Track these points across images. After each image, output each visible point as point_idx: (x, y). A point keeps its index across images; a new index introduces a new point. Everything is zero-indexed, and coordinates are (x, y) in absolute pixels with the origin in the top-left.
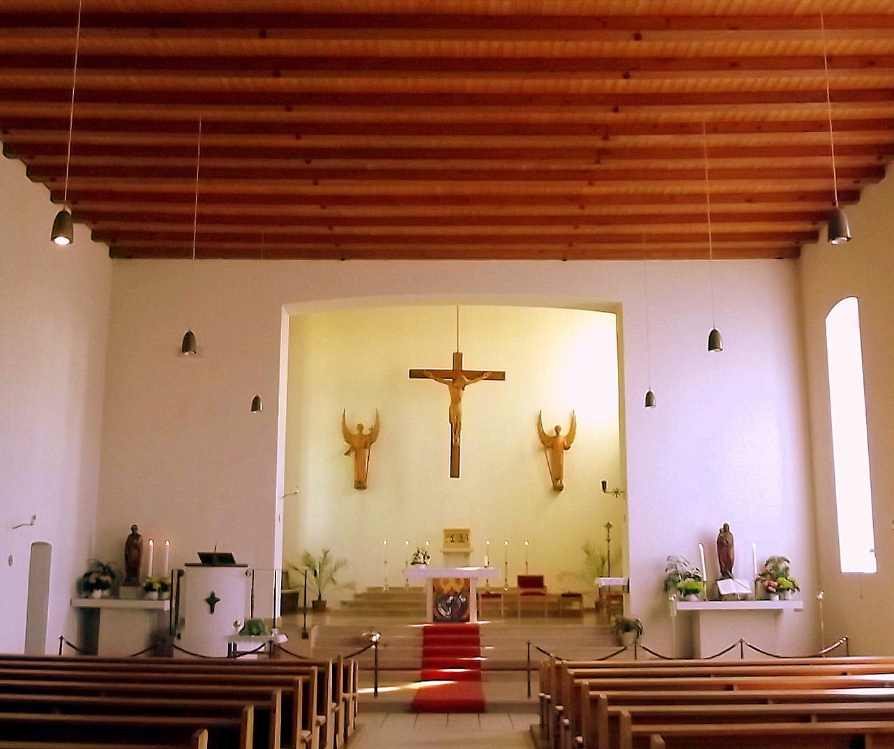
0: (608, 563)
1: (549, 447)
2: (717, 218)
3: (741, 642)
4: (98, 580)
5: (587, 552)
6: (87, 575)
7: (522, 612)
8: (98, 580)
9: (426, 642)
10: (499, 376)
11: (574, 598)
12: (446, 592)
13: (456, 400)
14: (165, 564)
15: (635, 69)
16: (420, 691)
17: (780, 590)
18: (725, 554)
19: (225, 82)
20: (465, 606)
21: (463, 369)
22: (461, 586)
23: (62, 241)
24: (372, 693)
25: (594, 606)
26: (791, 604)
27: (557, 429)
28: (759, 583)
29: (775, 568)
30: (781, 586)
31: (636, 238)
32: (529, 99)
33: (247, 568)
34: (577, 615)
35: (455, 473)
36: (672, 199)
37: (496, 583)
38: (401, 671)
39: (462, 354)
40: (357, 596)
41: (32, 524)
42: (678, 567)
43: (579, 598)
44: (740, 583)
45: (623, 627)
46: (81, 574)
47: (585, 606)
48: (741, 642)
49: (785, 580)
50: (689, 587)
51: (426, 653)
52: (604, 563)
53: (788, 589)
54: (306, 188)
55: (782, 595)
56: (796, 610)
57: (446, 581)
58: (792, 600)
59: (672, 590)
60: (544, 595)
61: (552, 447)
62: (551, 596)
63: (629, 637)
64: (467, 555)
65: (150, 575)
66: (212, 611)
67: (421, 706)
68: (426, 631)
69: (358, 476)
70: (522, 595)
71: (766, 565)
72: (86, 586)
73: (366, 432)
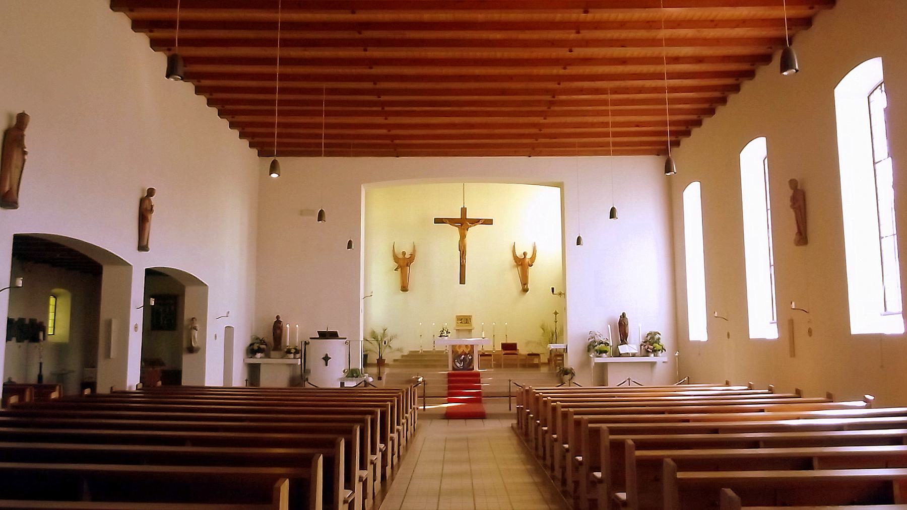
0: (555, 335)
1: (519, 265)
2: (615, 135)
3: (629, 379)
4: (259, 347)
5: (543, 329)
6: (252, 345)
7: (504, 364)
8: (259, 347)
9: (449, 382)
10: (489, 222)
11: (535, 356)
12: (459, 353)
13: (463, 237)
14: (296, 336)
15: (570, 65)
16: (448, 407)
17: (655, 351)
18: (623, 331)
19: (340, 70)
20: (471, 361)
21: (467, 217)
22: (469, 350)
23: (274, 176)
24: (422, 409)
25: (547, 361)
26: (661, 359)
27: (525, 254)
28: (643, 347)
29: (652, 338)
30: (655, 349)
31: (572, 145)
32: (510, 78)
33: (346, 340)
34: (536, 366)
35: (462, 281)
36: (593, 125)
37: (488, 348)
38: (437, 397)
39: (466, 208)
40: (403, 356)
41: (227, 316)
42: (596, 338)
43: (538, 356)
44: (632, 347)
45: (564, 372)
46: (249, 344)
47: (542, 361)
48: (629, 379)
49: (658, 345)
50: (602, 349)
51: (449, 388)
52: (553, 335)
53: (659, 351)
54: (380, 120)
55: (656, 354)
56: (664, 362)
57: (460, 346)
58: (662, 356)
59: (592, 350)
60: (517, 354)
61: (522, 265)
62: (521, 355)
63: (567, 377)
64: (470, 331)
65: (288, 344)
66: (327, 365)
67: (450, 416)
68: (449, 375)
69: (403, 283)
70: (504, 354)
71: (647, 336)
72: (252, 351)
73: (407, 256)
